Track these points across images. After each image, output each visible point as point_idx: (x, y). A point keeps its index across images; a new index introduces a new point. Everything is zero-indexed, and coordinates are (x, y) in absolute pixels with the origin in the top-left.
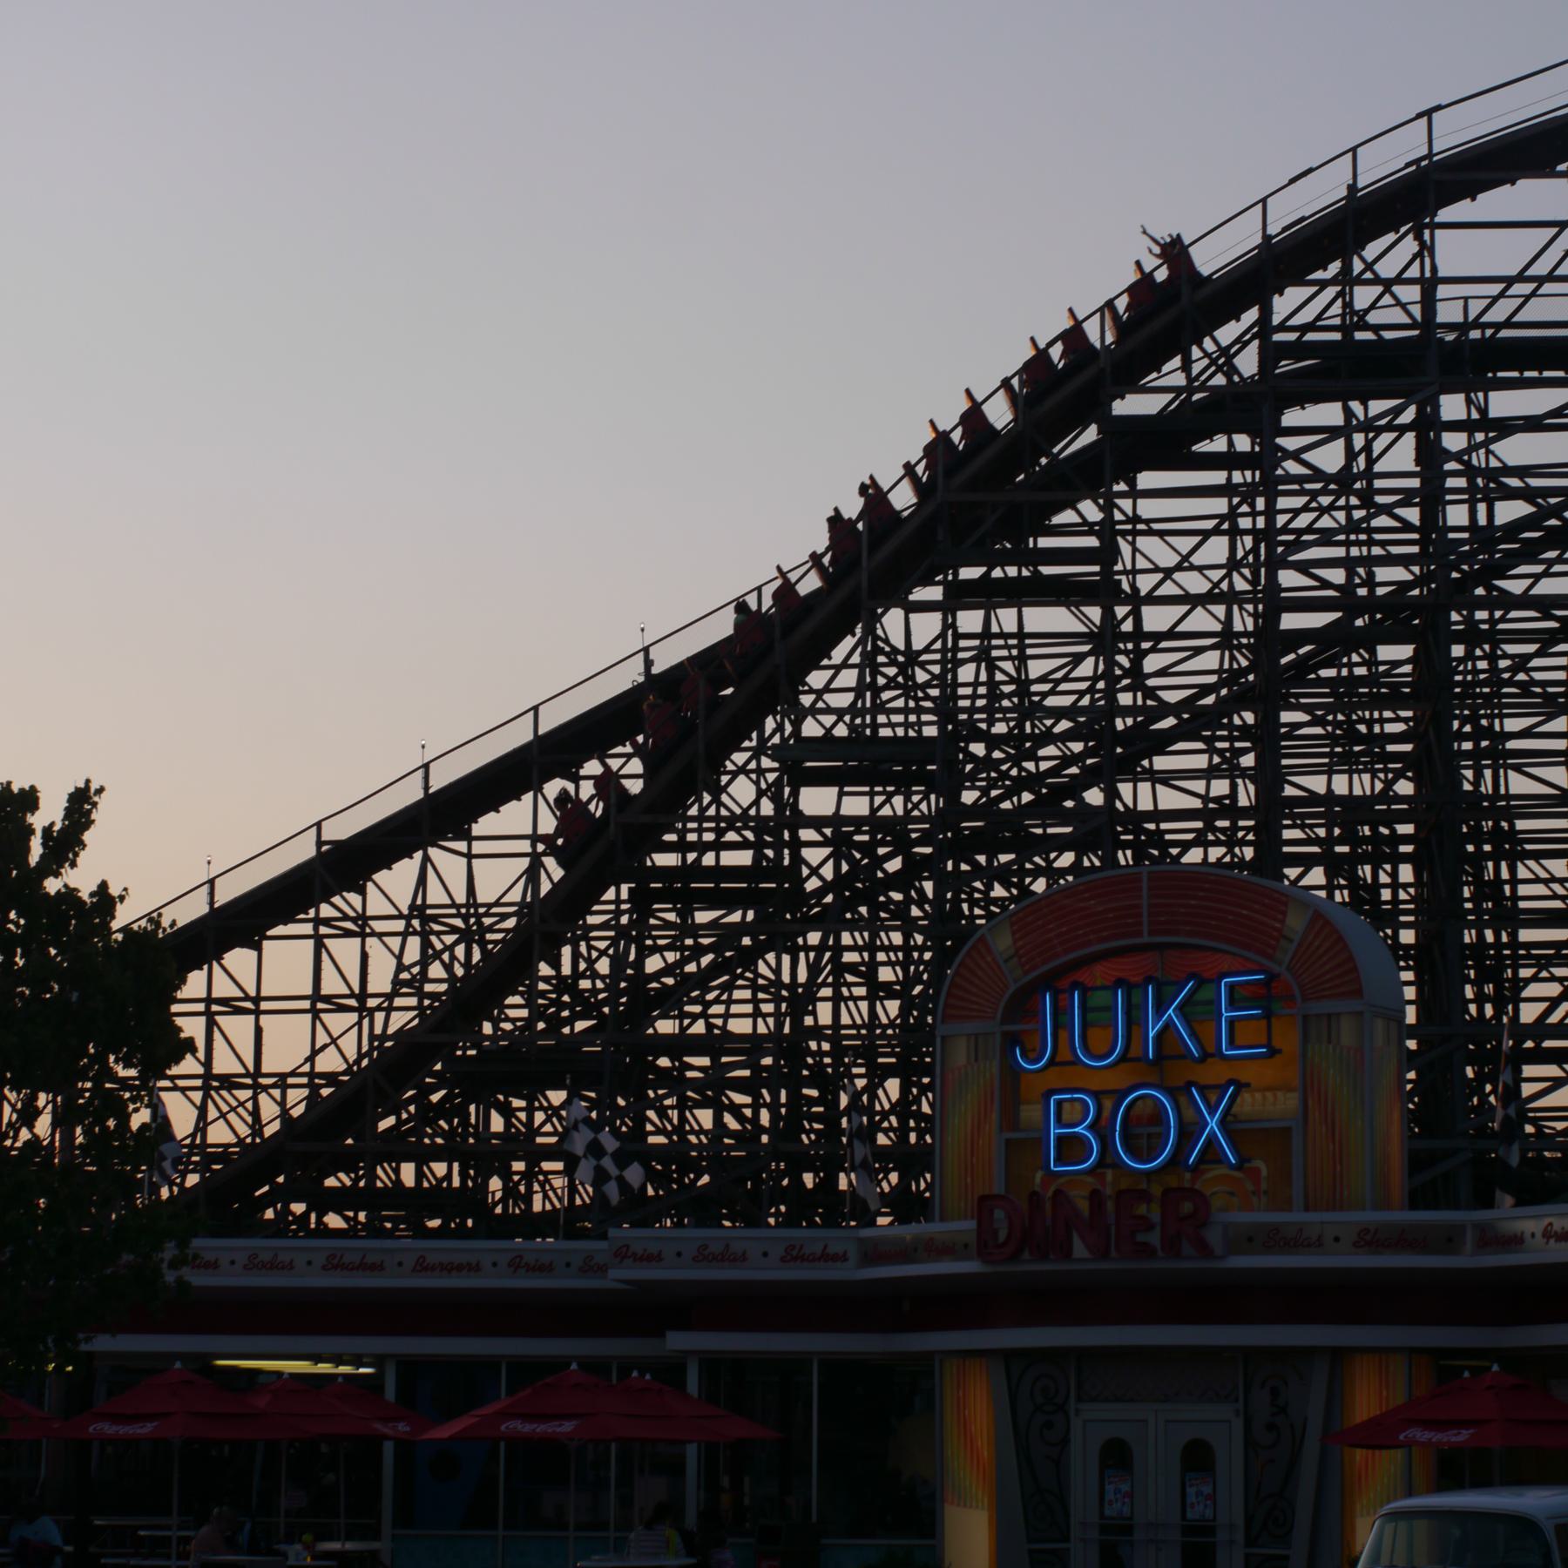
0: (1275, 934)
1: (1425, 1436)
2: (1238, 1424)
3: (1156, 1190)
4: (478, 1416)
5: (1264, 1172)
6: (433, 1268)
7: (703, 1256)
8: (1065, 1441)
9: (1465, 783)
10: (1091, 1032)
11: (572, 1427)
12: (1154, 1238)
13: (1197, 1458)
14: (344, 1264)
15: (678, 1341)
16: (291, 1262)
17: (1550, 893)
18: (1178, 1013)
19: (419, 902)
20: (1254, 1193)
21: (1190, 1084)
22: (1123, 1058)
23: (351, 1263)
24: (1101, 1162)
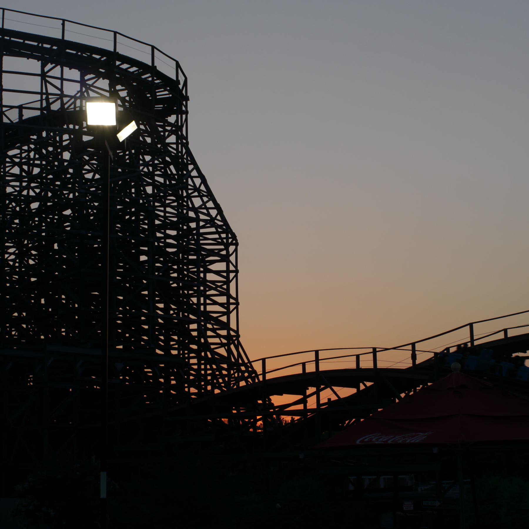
9: (120, 63)
17: (235, 310)
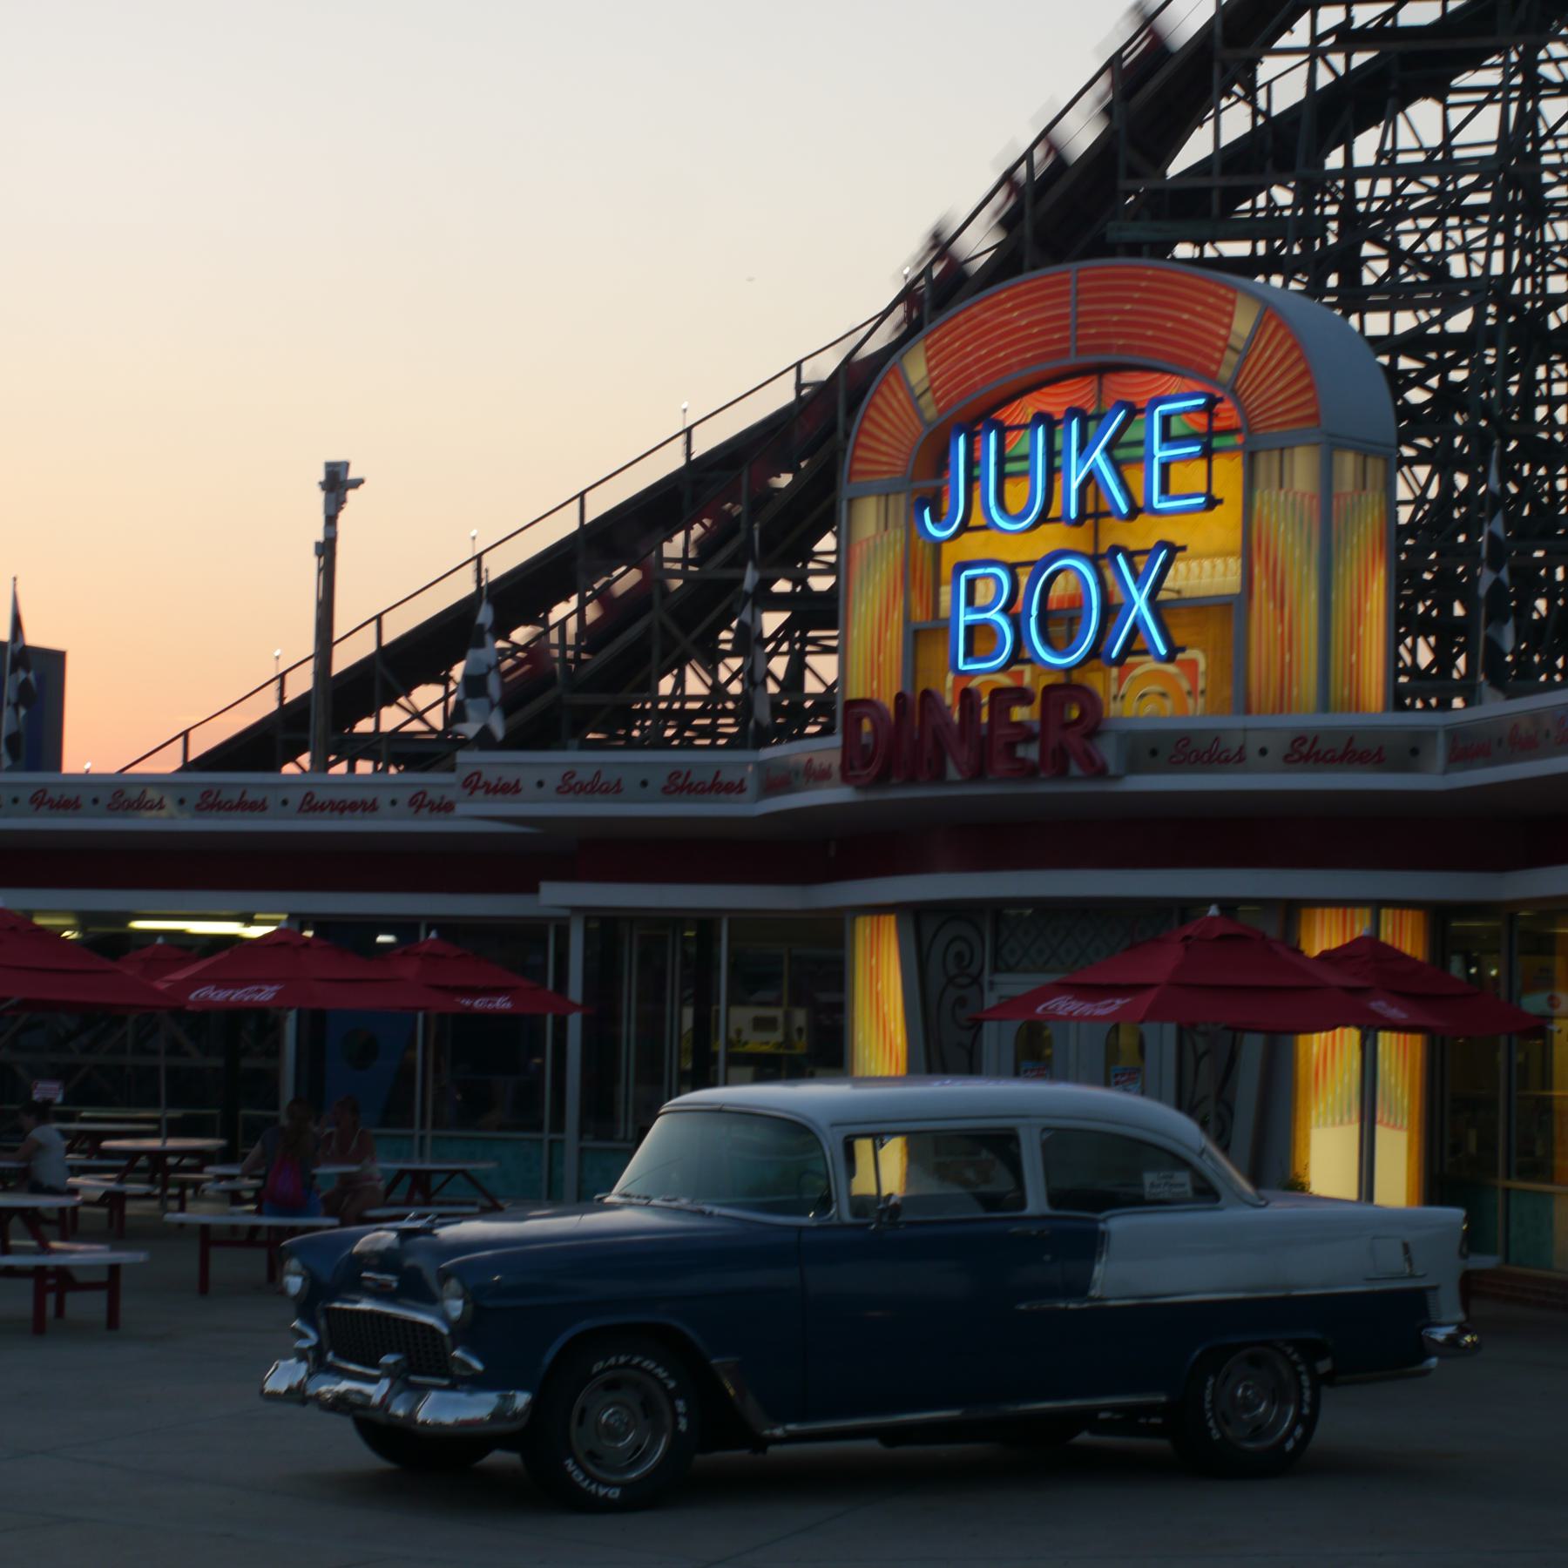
0: (1220, 344)
1: (220, 995)
4: (171, 981)
5: (1202, 666)
6: (322, 808)
7: (419, 802)
10: (1009, 487)
11: (272, 995)
14: (691, 784)
15: (555, 896)
16: (264, 801)
18: (1105, 455)
19: (1388, 146)
20: (1189, 693)
21: (1115, 550)
22: (1043, 518)
23: (341, 802)
24: (1015, 658)
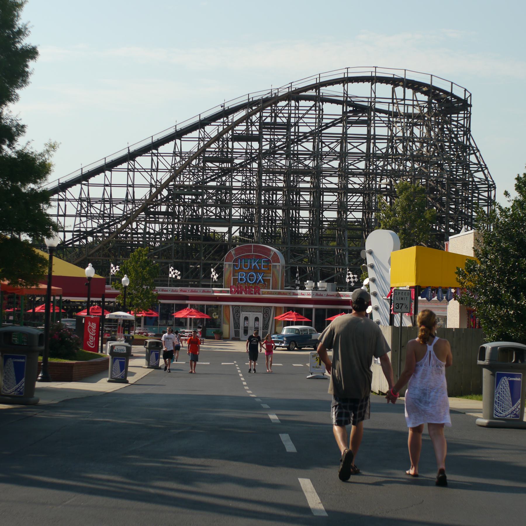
2: (262, 315)
3: (253, 286)
8: (240, 317)
12: (253, 292)
13: (257, 319)
22: (249, 268)
24: (246, 282)
